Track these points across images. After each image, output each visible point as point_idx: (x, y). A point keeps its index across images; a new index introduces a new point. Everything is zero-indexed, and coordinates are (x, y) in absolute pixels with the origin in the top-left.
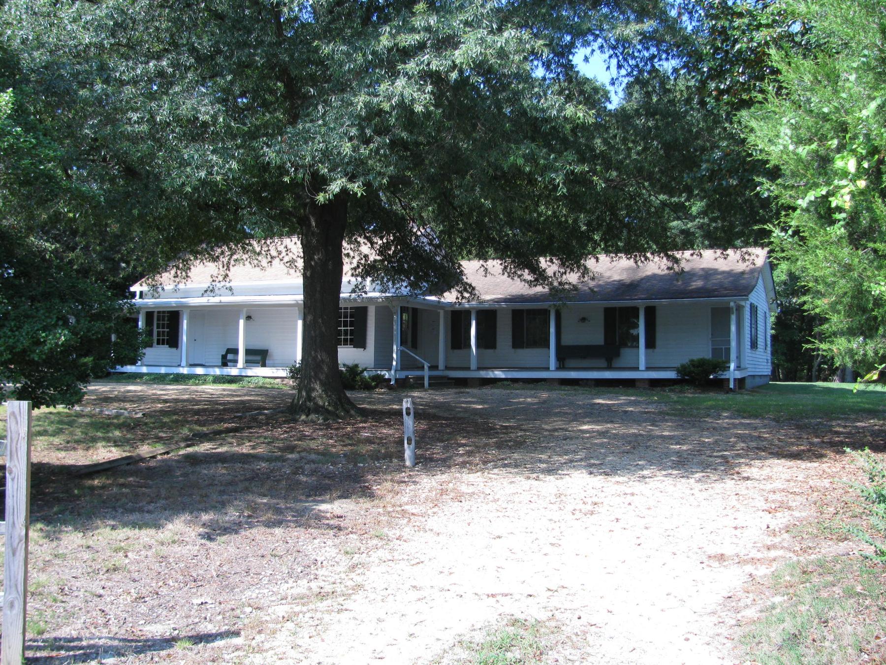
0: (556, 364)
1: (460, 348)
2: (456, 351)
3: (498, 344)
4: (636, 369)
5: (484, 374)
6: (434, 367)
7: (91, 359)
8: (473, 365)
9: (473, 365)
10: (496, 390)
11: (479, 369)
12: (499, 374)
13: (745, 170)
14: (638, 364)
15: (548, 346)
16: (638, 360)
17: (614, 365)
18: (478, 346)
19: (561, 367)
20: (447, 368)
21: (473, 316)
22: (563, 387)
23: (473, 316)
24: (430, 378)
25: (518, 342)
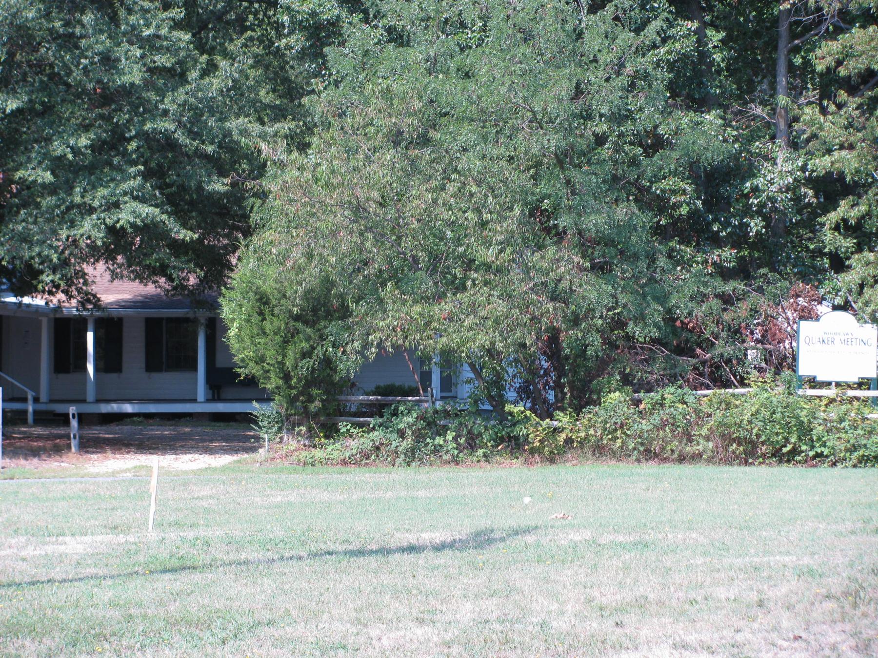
0: (206, 394)
1: (66, 370)
2: (156, 376)
3: (125, 366)
4: (194, 401)
5: (105, 408)
6: (36, 400)
7: (144, 34)
8: (91, 395)
9: (91, 395)
10: (125, 427)
11: (98, 401)
12: (128, 408)
13: (768, 28)
14: (196, 394)
15: (194, 368)
16: (196, 389)
17: (223, 396)
18: (97, 369)
19: (215, 394)
20: (52, 401)
21: (90, 326)
22: (213, 424)
23: (90, 326)
24: (35, 412)
25: (153, 365)
